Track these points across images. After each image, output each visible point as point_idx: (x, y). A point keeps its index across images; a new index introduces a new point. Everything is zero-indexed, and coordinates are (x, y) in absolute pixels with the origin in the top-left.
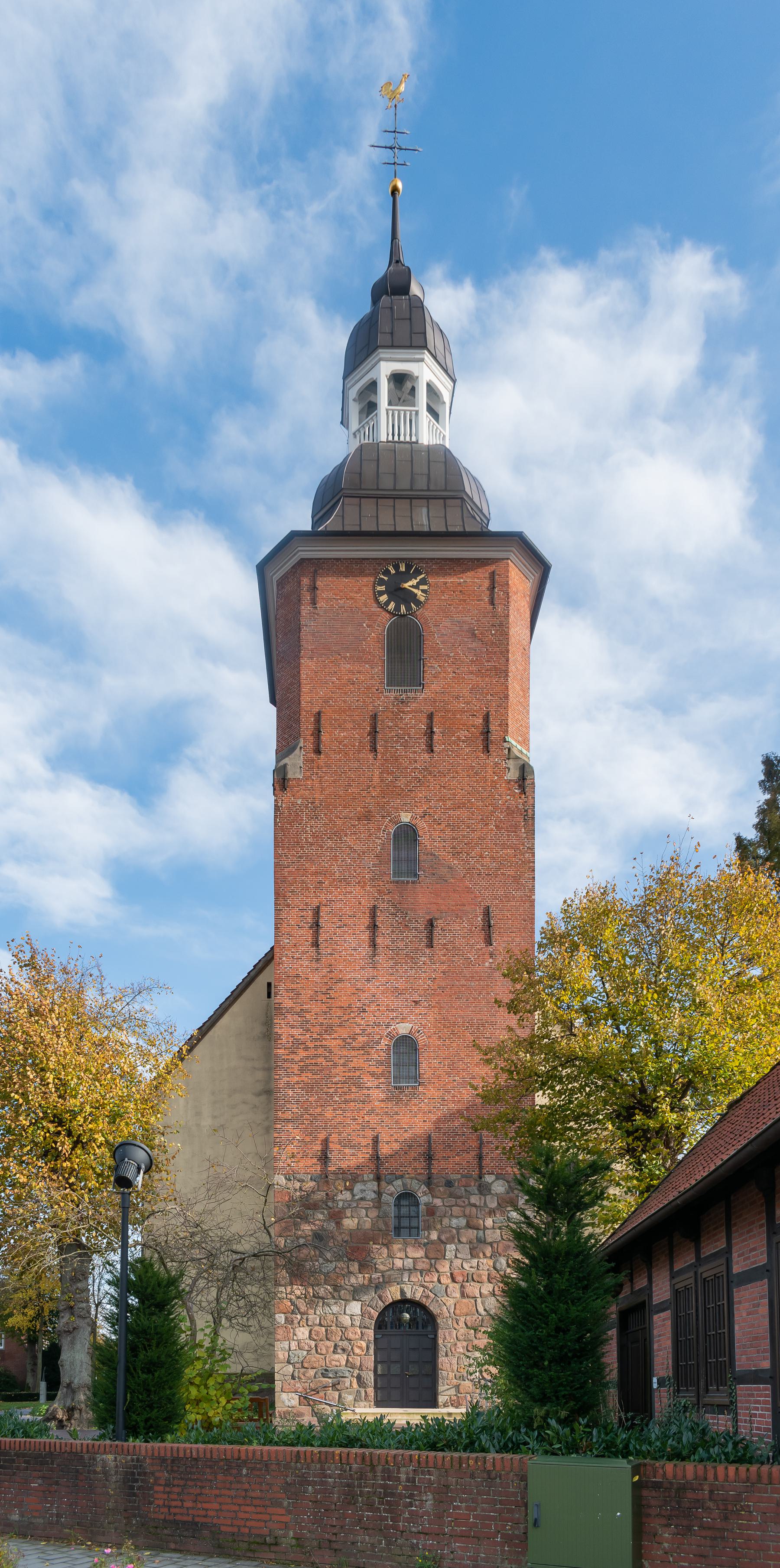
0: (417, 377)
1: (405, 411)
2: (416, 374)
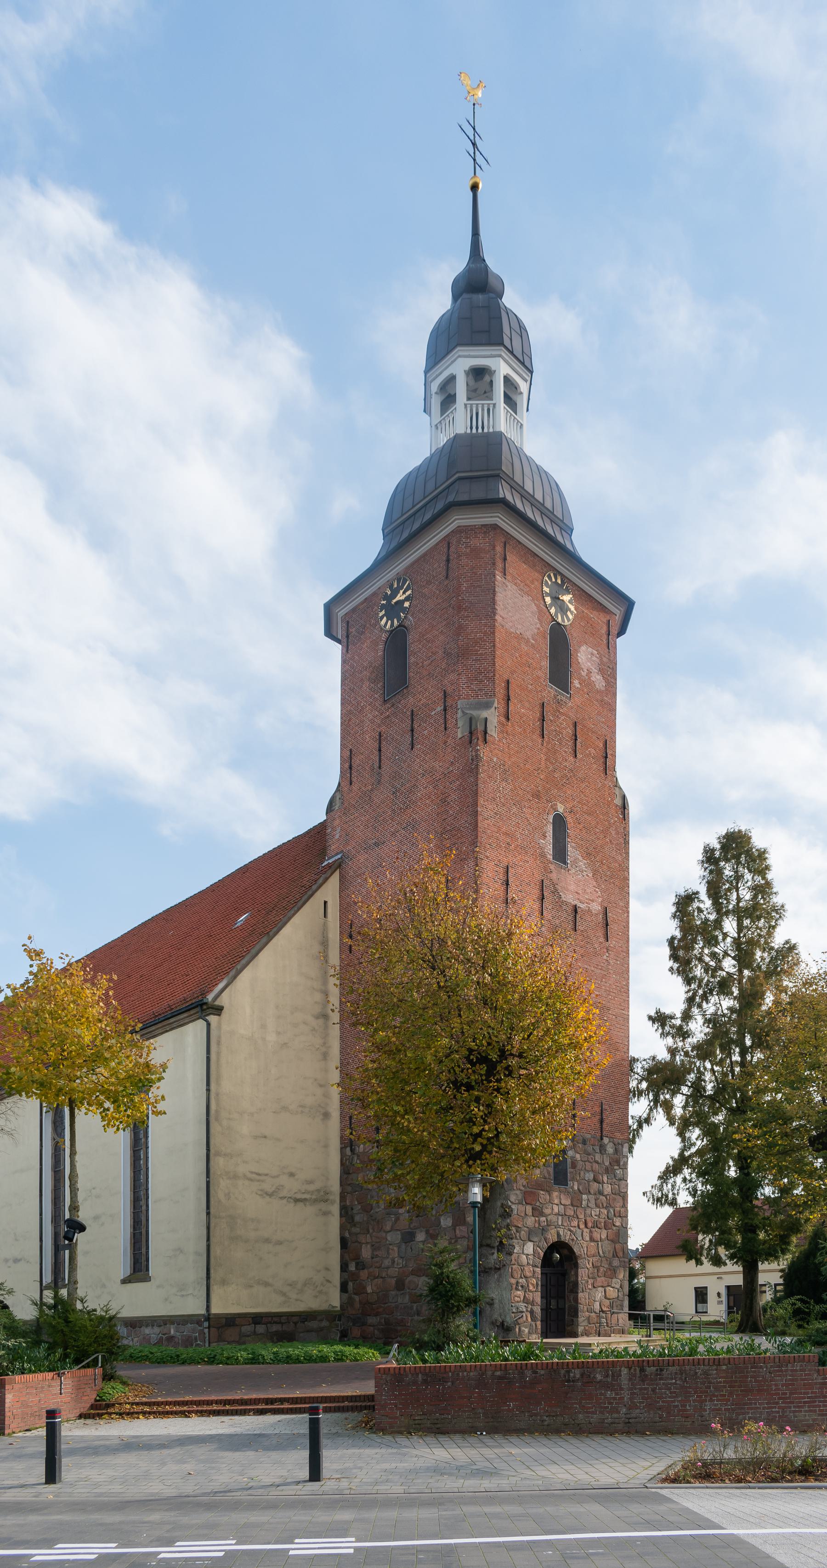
0: (495, 371)
1: (483, 405)
2: (493, 369)
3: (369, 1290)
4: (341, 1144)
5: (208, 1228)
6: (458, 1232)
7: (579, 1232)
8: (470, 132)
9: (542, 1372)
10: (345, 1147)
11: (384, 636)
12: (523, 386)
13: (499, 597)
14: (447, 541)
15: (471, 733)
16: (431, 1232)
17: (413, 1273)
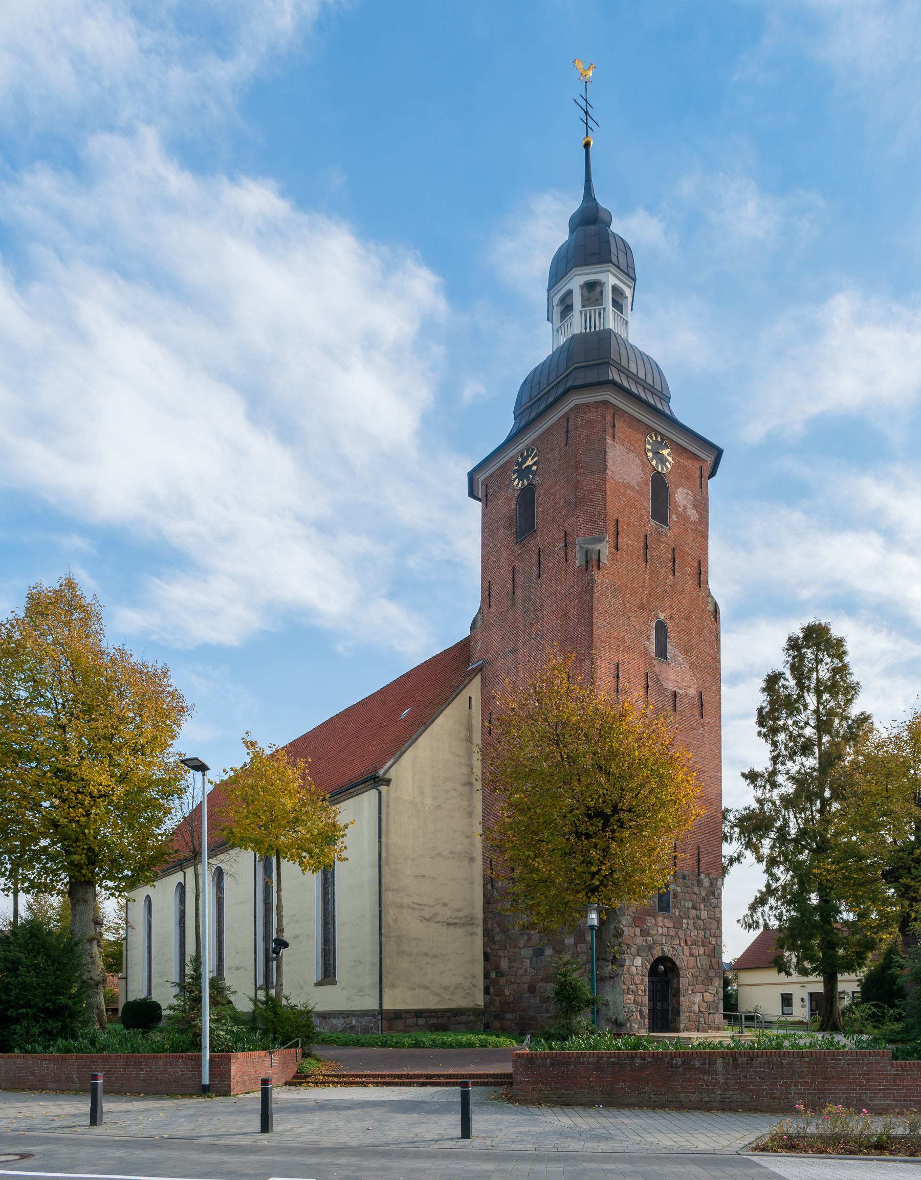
2: (603, 281)
3: (507, 993)
4: (484, 881)
5: (381, 945)
6: (579, 948)
7: (680, 949)
8: (583, 104)
9: (650, 1059)
10: (487, 884)
11: (516, 494)
12: (628, 292)
13: (610, 456)
14: (567, 417)
15: (587, 562)
16: (557, 948)
17: (542, 980)
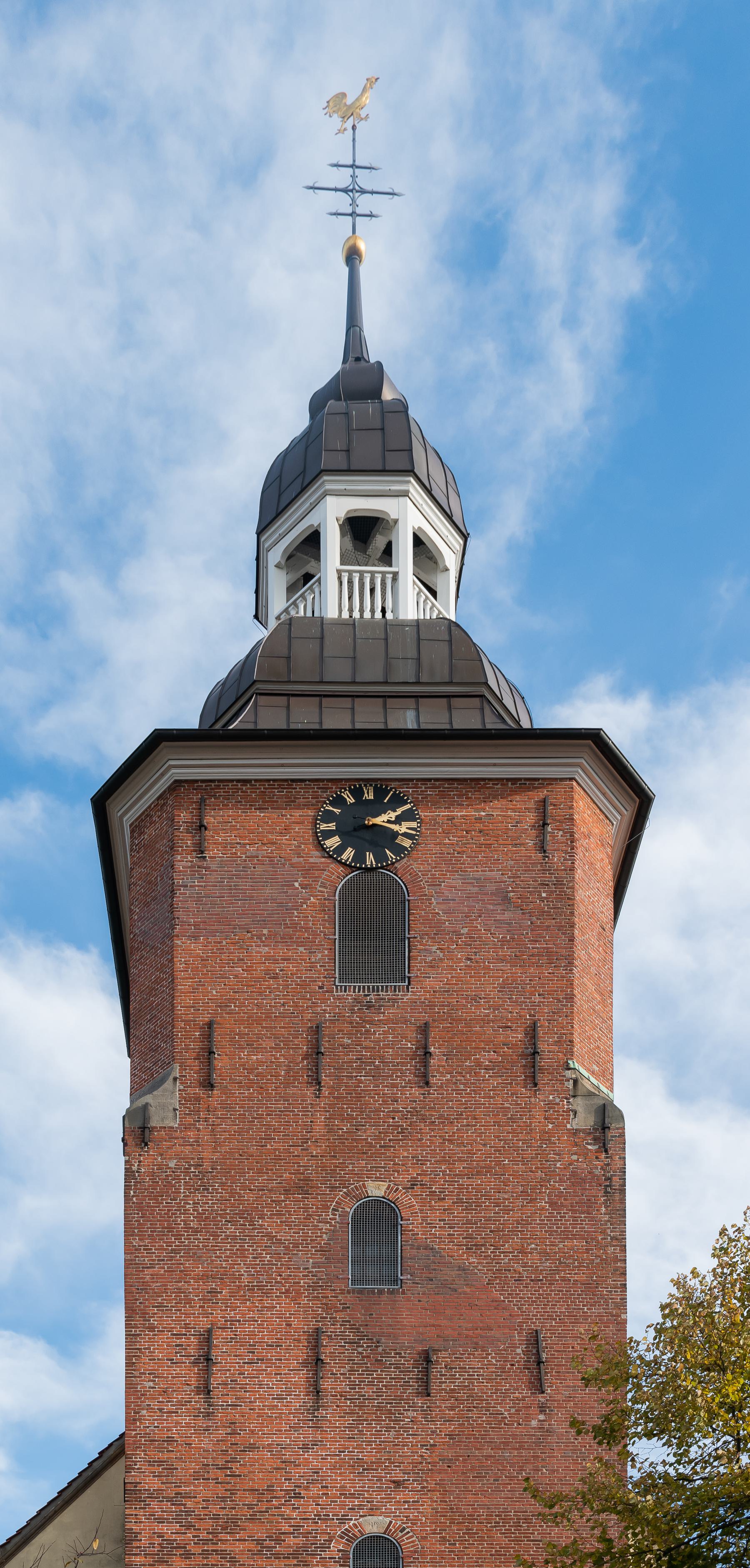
0: (396, 521)
